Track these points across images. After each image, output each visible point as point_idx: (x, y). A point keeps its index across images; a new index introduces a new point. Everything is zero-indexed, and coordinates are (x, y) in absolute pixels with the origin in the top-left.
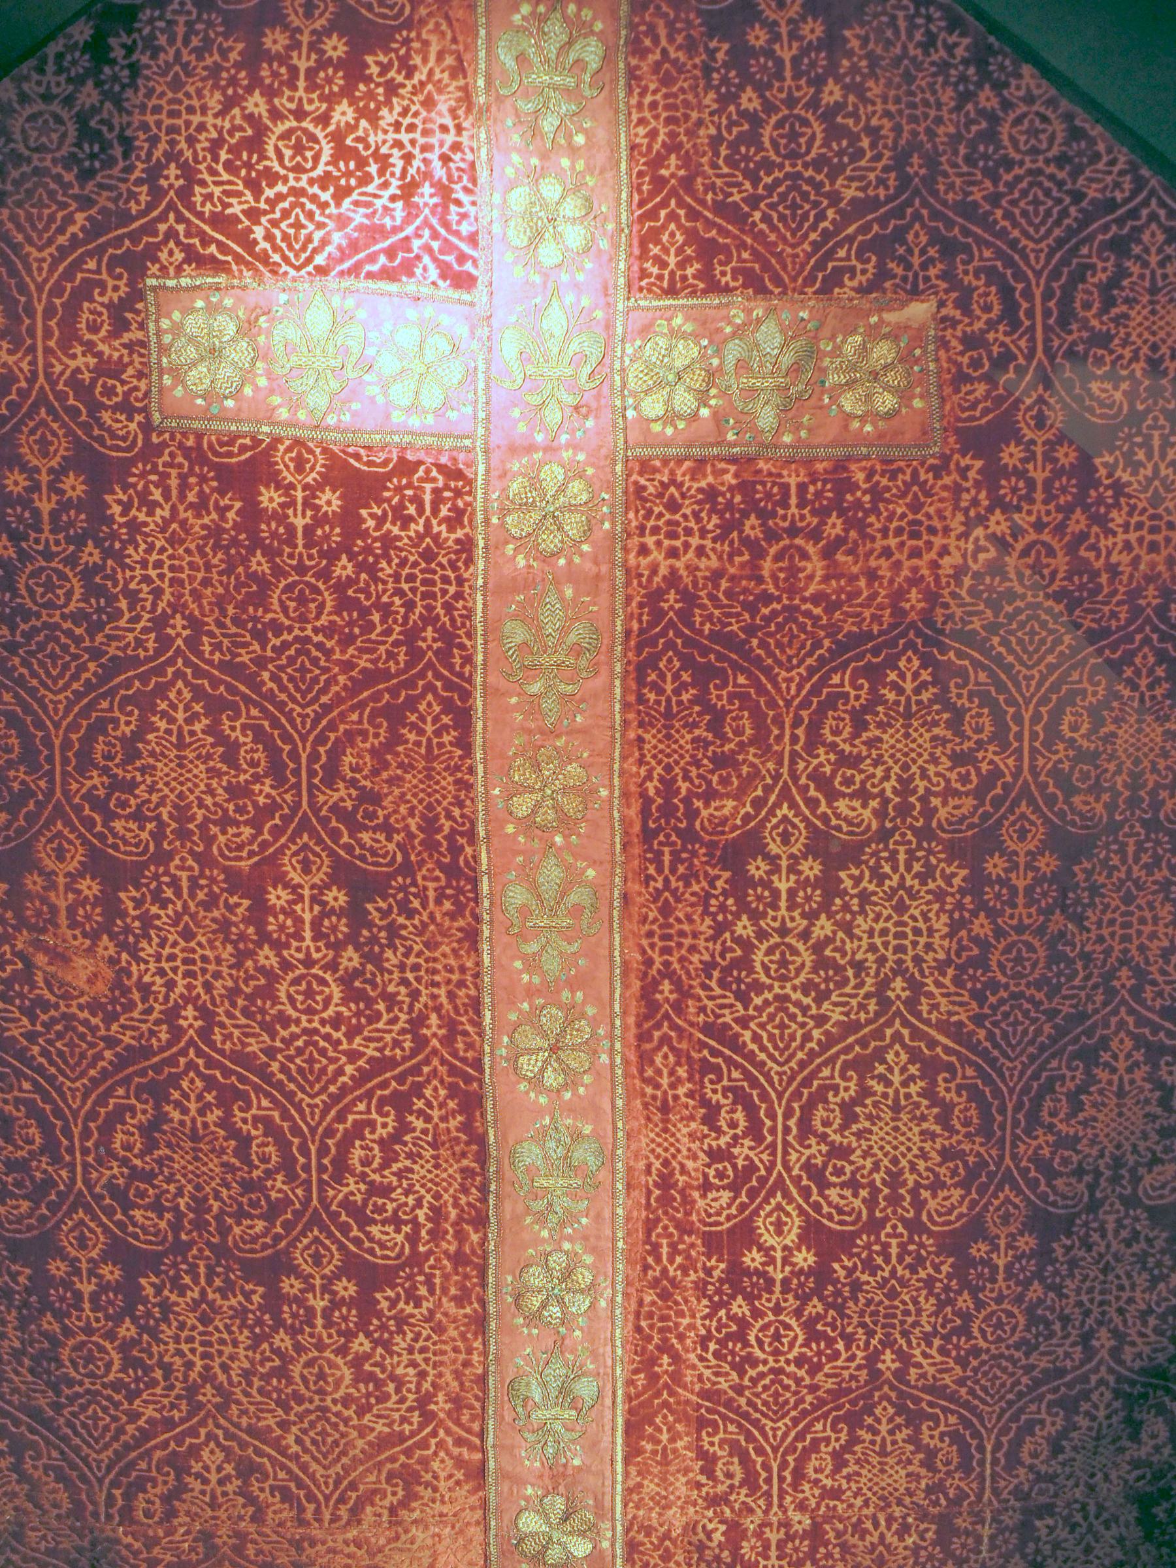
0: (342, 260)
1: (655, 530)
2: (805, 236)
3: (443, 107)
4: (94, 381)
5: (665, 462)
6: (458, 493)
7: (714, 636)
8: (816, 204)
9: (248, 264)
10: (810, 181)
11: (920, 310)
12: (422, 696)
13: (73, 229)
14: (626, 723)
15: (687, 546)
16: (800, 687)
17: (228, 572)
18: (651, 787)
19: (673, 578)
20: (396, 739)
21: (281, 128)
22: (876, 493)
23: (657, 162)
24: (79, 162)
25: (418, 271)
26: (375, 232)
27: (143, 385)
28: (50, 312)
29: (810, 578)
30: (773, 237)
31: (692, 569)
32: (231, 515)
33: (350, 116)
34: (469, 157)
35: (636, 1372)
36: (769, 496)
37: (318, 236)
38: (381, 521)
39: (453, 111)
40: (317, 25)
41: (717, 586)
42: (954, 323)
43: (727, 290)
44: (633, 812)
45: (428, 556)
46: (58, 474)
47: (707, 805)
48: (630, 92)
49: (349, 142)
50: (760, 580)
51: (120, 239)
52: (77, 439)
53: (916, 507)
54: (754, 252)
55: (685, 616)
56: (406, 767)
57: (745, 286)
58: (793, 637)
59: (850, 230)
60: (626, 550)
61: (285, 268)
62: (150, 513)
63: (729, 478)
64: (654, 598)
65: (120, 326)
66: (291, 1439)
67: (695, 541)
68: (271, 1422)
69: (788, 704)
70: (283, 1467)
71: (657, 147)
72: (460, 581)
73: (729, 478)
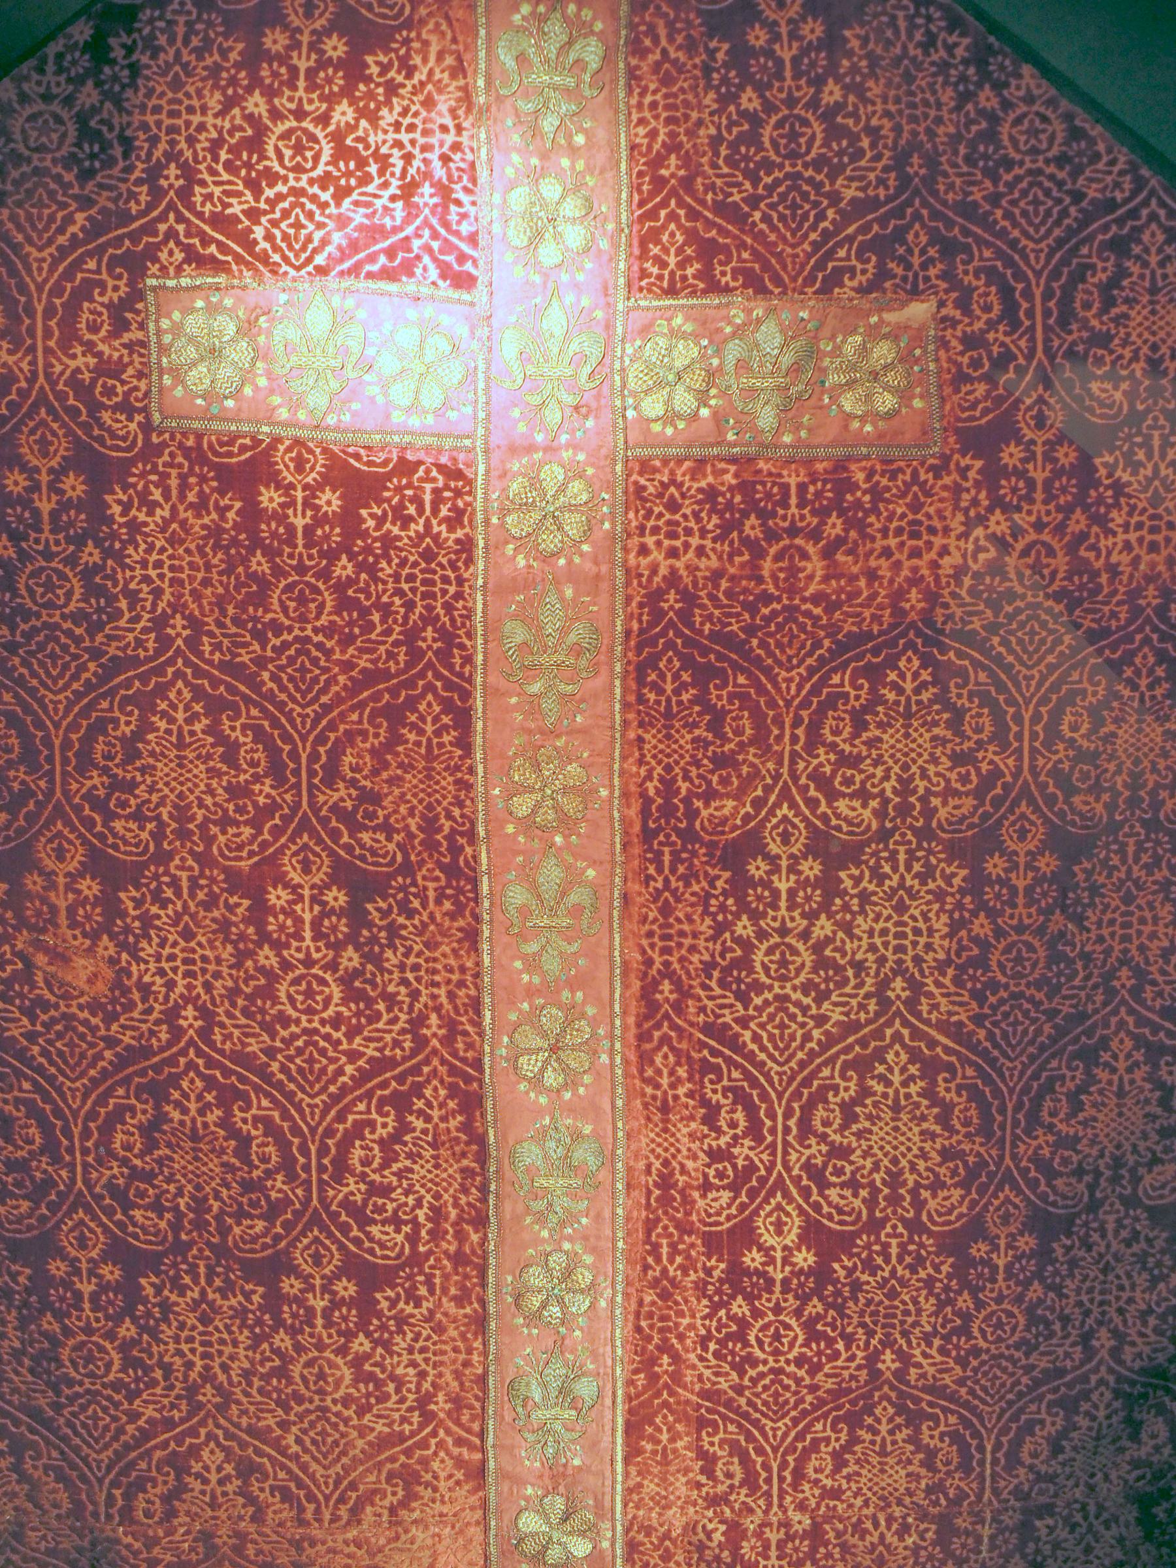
0: (342, 260)
1: (655, 530)
2: (805, 236)
3: (443, 107)
4: (94, 381)
5: (665, 462)
6: (458, 493)
7: (714, 636)
8: (816, 204)
9: (248, 264)
10: (810, 181)
11: (920, 310)
12: (422, 696)
13: (73, 229)
14: (626, 723)
15: (687, 546)
16: (800, 687)
17: (228, 572)
18: (651, 787)
19: (673, 578)
20: (396, 739)
21: (281, 128)
22: (876, 493)
23: (657, 162)
24: (79, 162)
25: (418, 271)
26: (375, 232)
27: (143, 385)
28: (50, 312)
29: (810, 578)
30: (773, 237)
31: (692, 569)
32: (231, 515)
33: (350, 116)
34: (469, 157)
35: (636, 1372)
36: (769, 496)
37: (318, 236)
38: (381, 521)
39: (453, 111)
40: (317, 25)
41: (717, 586)
42: (954, 323)
43: (727, 290)
44: (633, 812)
45: (428, 556)
46: (58, 474)
47: (707, 805)
48: (630, 92)
49: (349, 142)
50: (760, 580)
51: (120, 239)
52: (77, 439)
53: (916, 507)
54: (754, 252)
55: (685, 616)
56: (406, 767)
57: (745, 286)
58: (793, 637)
59: (850, 230)
60: (626, 550)
61: (285, 268)
62: (150, 513)
63: (729, 478)
64: (654, 598)
65: (120, 326)
66: (291, 1439)
67: (695, 541)
68: (271, 1422)
69: (788, 704)
70: (283, 1467)
71: (657, 147)
72: (460, 581)
73: (729, 478)
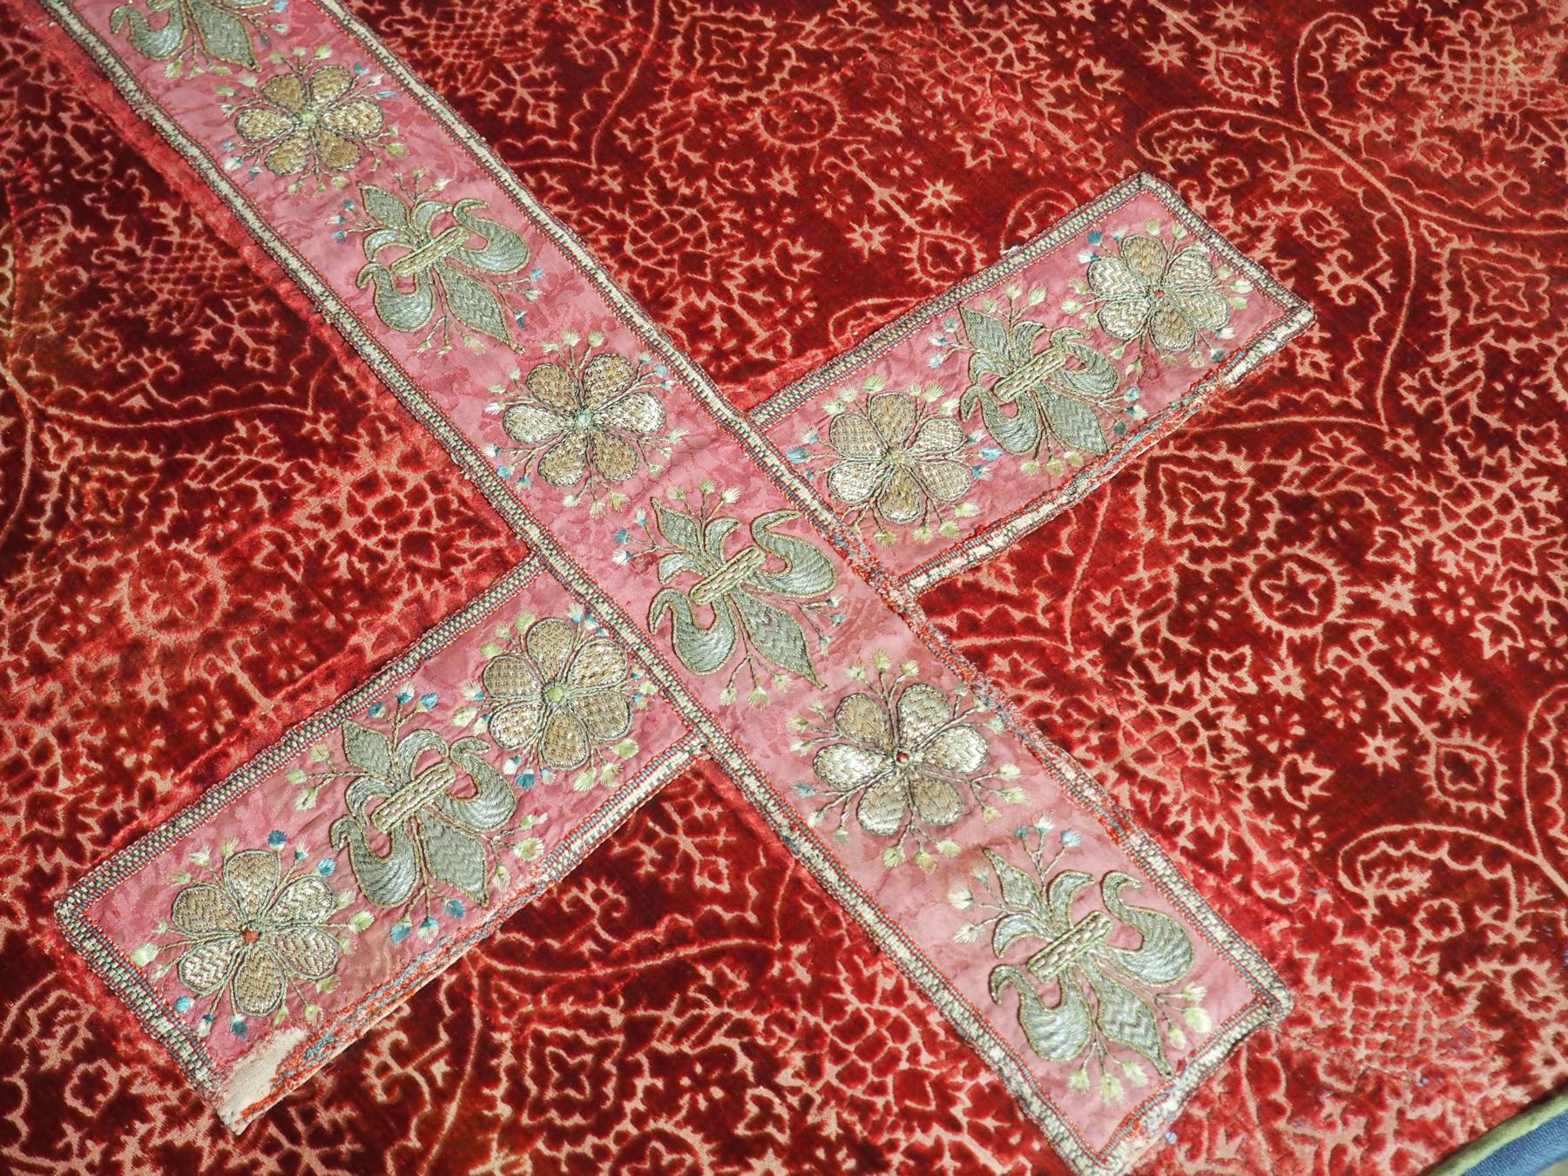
0: (1113, 511)
1: (417, 496)
2: (518, 1051)
3: (1173, 785)
4: (1255, 170)
5: (476, 592)
6: (719, 355)
7: (226, 426)
8: (539, 1108)
9: (1219, 419)
10: (576, 1136)
11: (245, 1093)
12: (562, 119)
13: (1446, 295)
14: (267, 255)
15: (356, 509)
16: (41, 451)
17: (914, 91)
18: (170, 212)
19: (342, 454)
20: (554, 52)
21: (1342, 598)
22: (121, 779)
23: (822, 957)
24: (1520, 372)
25: (1008, 568)
26: (1111, 570)
27: (1200, 207)
28: (1375, 198)
29: (138, 602)
30: (567, 1008)
31: (324, 485)
32: (967, 148)
33: (1275, 682)
34: (1080, 752)
36: (288, 658)
37: (1171, 517)
38: (786, 259)
39: (1157, 789)
40: (1430, 760)
41: (270, 492)
42: (175, 1118)
43: (575, 878)
44: (172, 173)
45: (693, 263)
46: (1194, 54)
47: (71, 240)
48: (950, 1030)
49: (1246, 650)
50: (213, 547)
51: (1387, 334)
52: (1211, 101)
53: (41, 807)
54: (580, 962)
55: (286, 423)
56: (511, 40)
57: (552, 903)
58: (105, 505)
59: (452, 1111)
60: (441, 445)
61: (1171, 450)
62: (1058, 92)
63: (364, 639)
64: (350, 414)
65: (1287, 244)
67: (350, 523)
69: (41, 416)
71: (843, 975)
72: (627, 264)
73: (364, 639)
